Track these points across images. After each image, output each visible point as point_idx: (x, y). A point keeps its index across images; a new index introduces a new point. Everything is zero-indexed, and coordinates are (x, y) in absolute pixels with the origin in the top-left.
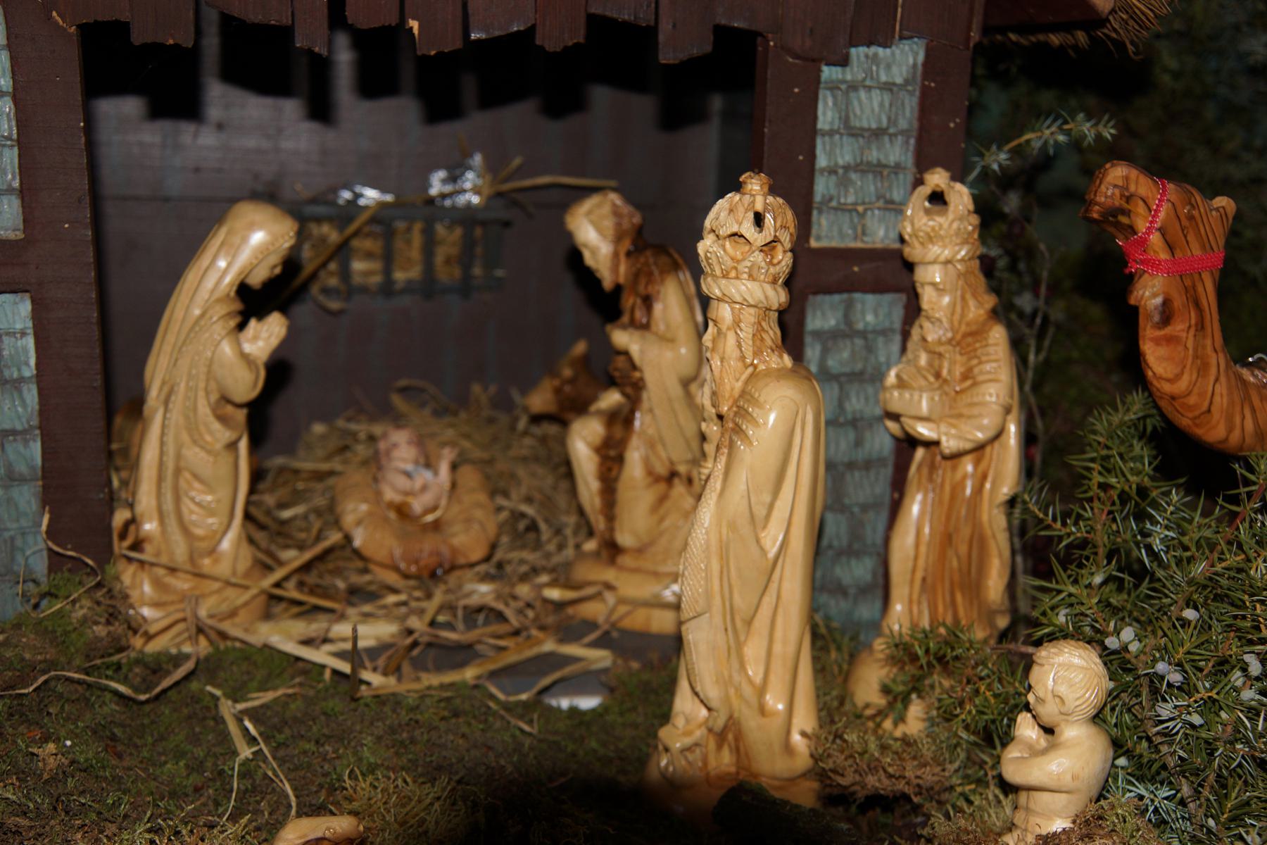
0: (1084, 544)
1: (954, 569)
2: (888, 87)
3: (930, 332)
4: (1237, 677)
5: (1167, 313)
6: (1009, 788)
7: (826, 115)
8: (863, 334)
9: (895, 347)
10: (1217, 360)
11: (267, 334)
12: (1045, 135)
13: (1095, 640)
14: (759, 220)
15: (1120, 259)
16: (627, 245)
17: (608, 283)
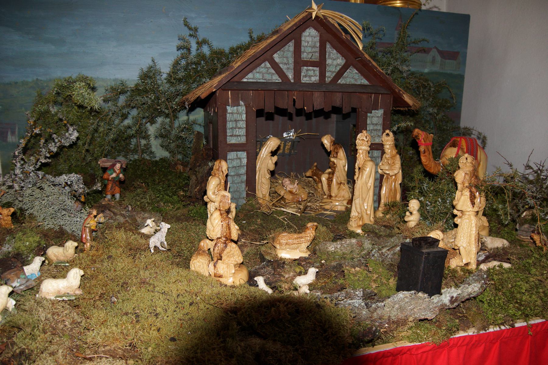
0: (415, 186)
1: (392, 192)
2: (378, 117)
3: (387, 156)
4: (438, 203)
5: (424, 152)
6: (407, 222)
7: (369, 122)
8: (374, 157)
9: (380, 159)
10: (432, 159)
11: (275, 158)
12: (403, 125)
13: (418, 199)
14: (366, 137)
15: (417, 143)
16: (332, 143)
17: (329, 150)
